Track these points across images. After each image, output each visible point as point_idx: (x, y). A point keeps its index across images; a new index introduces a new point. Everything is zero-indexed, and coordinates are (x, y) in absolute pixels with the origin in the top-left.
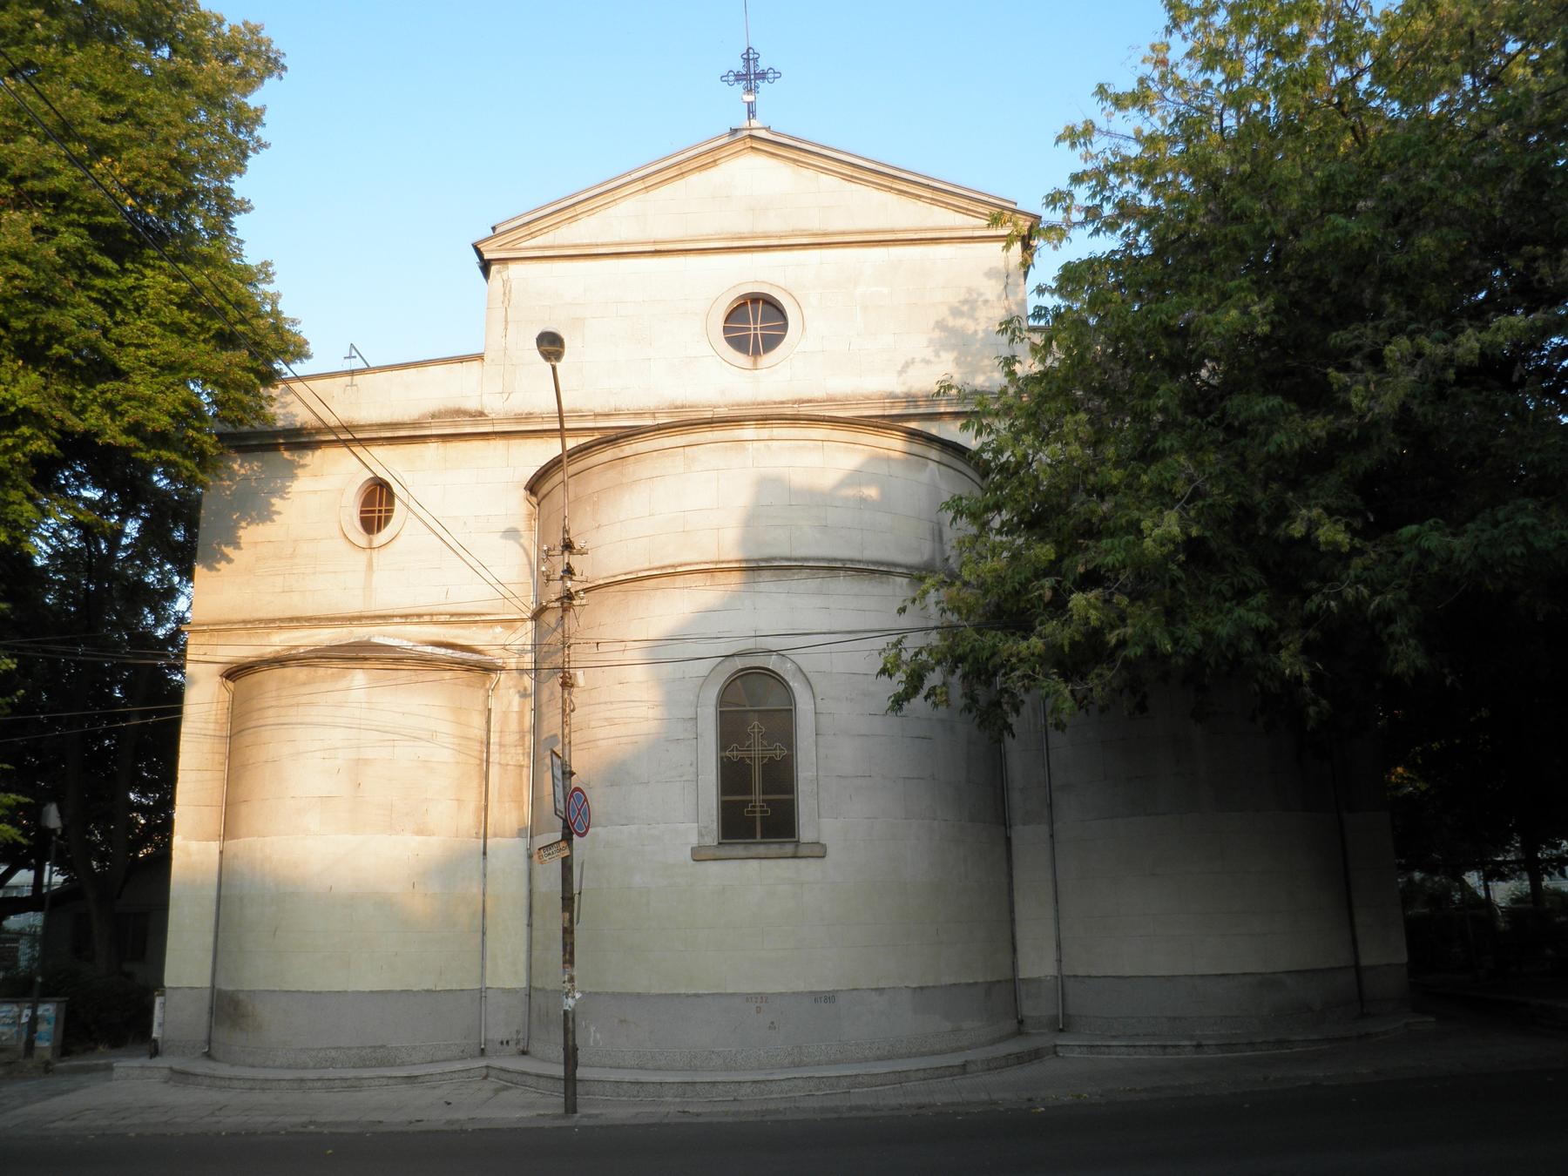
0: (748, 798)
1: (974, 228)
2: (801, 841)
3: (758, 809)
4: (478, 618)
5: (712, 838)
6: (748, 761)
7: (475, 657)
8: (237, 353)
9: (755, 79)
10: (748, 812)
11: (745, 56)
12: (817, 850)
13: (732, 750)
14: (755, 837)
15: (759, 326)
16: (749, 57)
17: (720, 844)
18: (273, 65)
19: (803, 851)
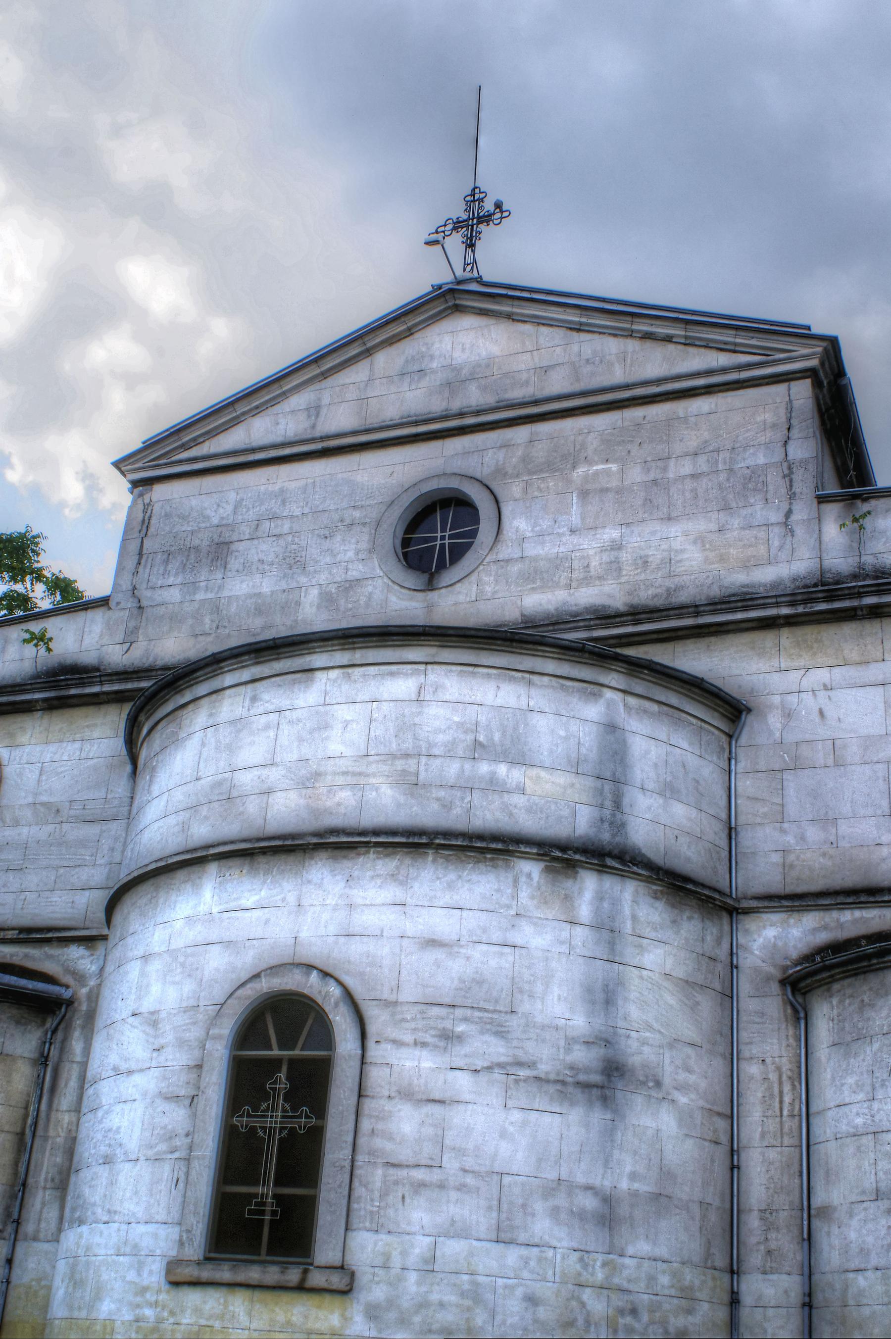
0: (251, 1190)
1: (724, 370)
2: (316, 1263)
3: (268, 1208)
4: (50, 935)
5: (196, 1249)
6: (261, 1134)
7: (41, 986)
8: (773, 949)
9: (478, 223)
10: (251, 1212)
11: (469, 198)
12: (337, 1281)
13: (242, 1116)
14: (259, 1255)
15: (438, 542)
16: (474, 197)
17: (207, 1259)
18: (749, 710)
19: (317, 1279)
